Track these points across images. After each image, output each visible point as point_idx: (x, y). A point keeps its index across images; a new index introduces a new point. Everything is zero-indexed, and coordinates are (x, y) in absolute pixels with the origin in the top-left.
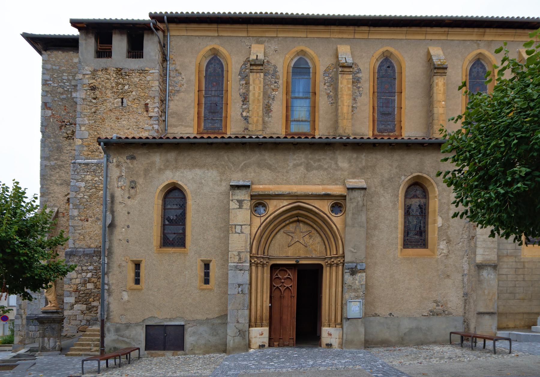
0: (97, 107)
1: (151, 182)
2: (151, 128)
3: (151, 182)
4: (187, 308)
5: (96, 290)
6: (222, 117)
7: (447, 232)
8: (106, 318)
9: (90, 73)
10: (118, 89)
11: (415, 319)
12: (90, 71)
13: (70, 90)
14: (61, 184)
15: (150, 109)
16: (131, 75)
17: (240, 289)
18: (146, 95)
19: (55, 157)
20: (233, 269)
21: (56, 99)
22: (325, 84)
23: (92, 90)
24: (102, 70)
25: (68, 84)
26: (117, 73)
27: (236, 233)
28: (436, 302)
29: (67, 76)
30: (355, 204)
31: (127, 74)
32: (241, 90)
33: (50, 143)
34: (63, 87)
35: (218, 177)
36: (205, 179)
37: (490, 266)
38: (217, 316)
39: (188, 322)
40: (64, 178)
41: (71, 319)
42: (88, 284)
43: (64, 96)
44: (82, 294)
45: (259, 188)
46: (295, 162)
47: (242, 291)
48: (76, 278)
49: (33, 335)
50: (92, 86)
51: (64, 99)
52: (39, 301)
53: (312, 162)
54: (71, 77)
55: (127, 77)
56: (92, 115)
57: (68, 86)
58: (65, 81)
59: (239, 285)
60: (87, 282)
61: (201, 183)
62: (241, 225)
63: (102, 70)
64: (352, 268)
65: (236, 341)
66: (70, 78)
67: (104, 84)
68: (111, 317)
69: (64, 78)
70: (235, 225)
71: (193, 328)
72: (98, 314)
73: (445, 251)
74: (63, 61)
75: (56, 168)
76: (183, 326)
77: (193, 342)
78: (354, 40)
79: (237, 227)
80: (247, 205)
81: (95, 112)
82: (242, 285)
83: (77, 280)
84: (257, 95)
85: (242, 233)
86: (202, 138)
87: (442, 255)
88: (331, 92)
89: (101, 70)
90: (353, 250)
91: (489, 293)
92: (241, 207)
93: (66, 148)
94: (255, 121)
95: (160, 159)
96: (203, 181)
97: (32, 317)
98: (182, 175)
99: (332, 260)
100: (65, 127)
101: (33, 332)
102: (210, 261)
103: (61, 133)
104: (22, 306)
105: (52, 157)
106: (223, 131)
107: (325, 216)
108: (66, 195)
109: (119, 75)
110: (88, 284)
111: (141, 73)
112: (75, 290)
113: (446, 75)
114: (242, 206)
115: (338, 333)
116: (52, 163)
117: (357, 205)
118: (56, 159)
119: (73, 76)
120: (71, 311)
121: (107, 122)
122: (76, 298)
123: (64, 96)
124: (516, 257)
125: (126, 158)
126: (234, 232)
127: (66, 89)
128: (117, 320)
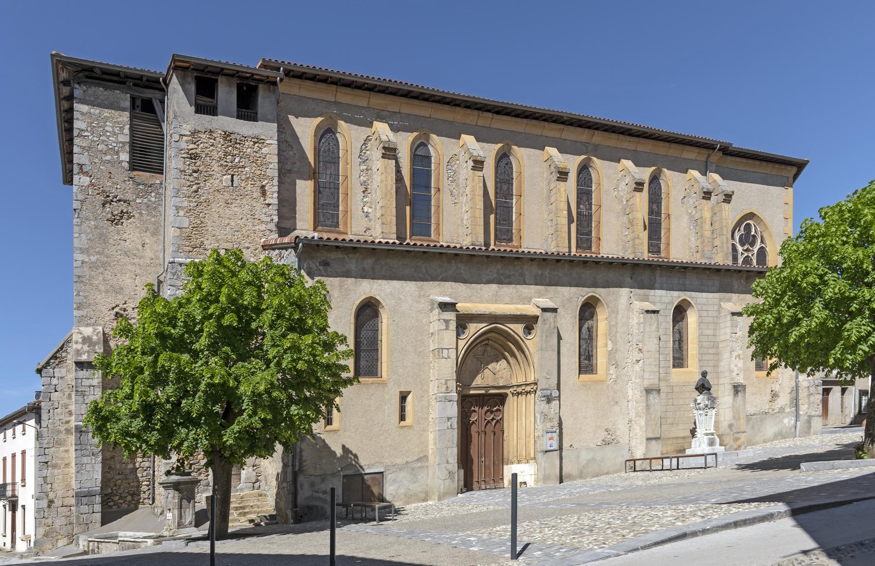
0: (199, 184)
1: (347, 295)
2: (268, 219)
3: (347, 295)
4: (386, 451)
6: (338, 211)
7: (616, 356)
8: (299, 470)
9: (190, 133)
10: (226, 162)
11: (591, 449)
12: (190, 131)
13: (116, 148)
14: (107, 292)
15: (268, 194)
16: (243, 143)
17: (449, 423)
18: (263, 173)
19: (97, 250)
20: (443, 400)
21: (96, 160)
22: (448, 179)
23: (191, 158)
24: (205, 132)
25: (113, 139)
26: (225, 139)
27: (443, 358)
28: (607, 430)
29: (112, 127)
30: (548, 326)
31: (238, 141)
32: (362, 178)
33: (89, 227)
34: (106, 143)
35: (416, 292)
36: (404, 294)
37: (655, 390)
38: (416, 458)
39: (387, 467)
40: (111, 283)
43: (108, 157)
45: (464, 307)
46: (488, 278)
47: (451, 425)
49: (86, 520)
50: (193, 154)
51: (109, 162)
52: (93, 467)
53: (503, 278)
54: (118, 128)
55: (238, 146)
56: (193, 195)
57: (114, 142)
58: (108, 134)
59: (449, 419)
61: (399, 299)
62: (448, 349)
63: (205, 132)
64: (548, 396)
65: (446, 484)
66: (117, 130)
67: (209, 152)
68: (304, 468)
69: (107, 128)
70: (442, 349)
71: (392, 475)
72: (209, 477)
73: (613, 377)
74: (106, 103)
75: (98, 266)
76: (382, 473)
77: (393, 492)
78: (476, 127)
79: (444, 351)
80: (453, 325)
81: (196, 191)
82: (451, 418)
84: (389, 187)
85: (449, 357)
86: (387, 243)
87: (612, 380)
88: (454, 188)
89: (203, 131)
90: (546, 375)
91: (655, 418)
92: (447, 328)
93: (113, 236)
94: (389, 221)
95: (356, 267)
96: (402, 296)
97: (84, 492)
98: (379, 287)
99: (523, 388)
100: (111, 204)
101: (86, 515)
102: (409, 392)
103: (104, 214)
104: (48, 479)
105: (93, 248)
106: (341, 230)
107: (519, 338)
108: (113, 309)
109: (228, 141)
111: (255, 143)
113: (566, 181)
114: (449, 326)
115: (533, 469)
116: (93, 258)
117: (550, 327)
118: (99, 253)
119: (120, 128)
121: (214, 207)
123: (108, 157)
124: (667, 381)
125: (318, 264)
126: (441, 357)
127: (111, 147)
128: (311, 471)
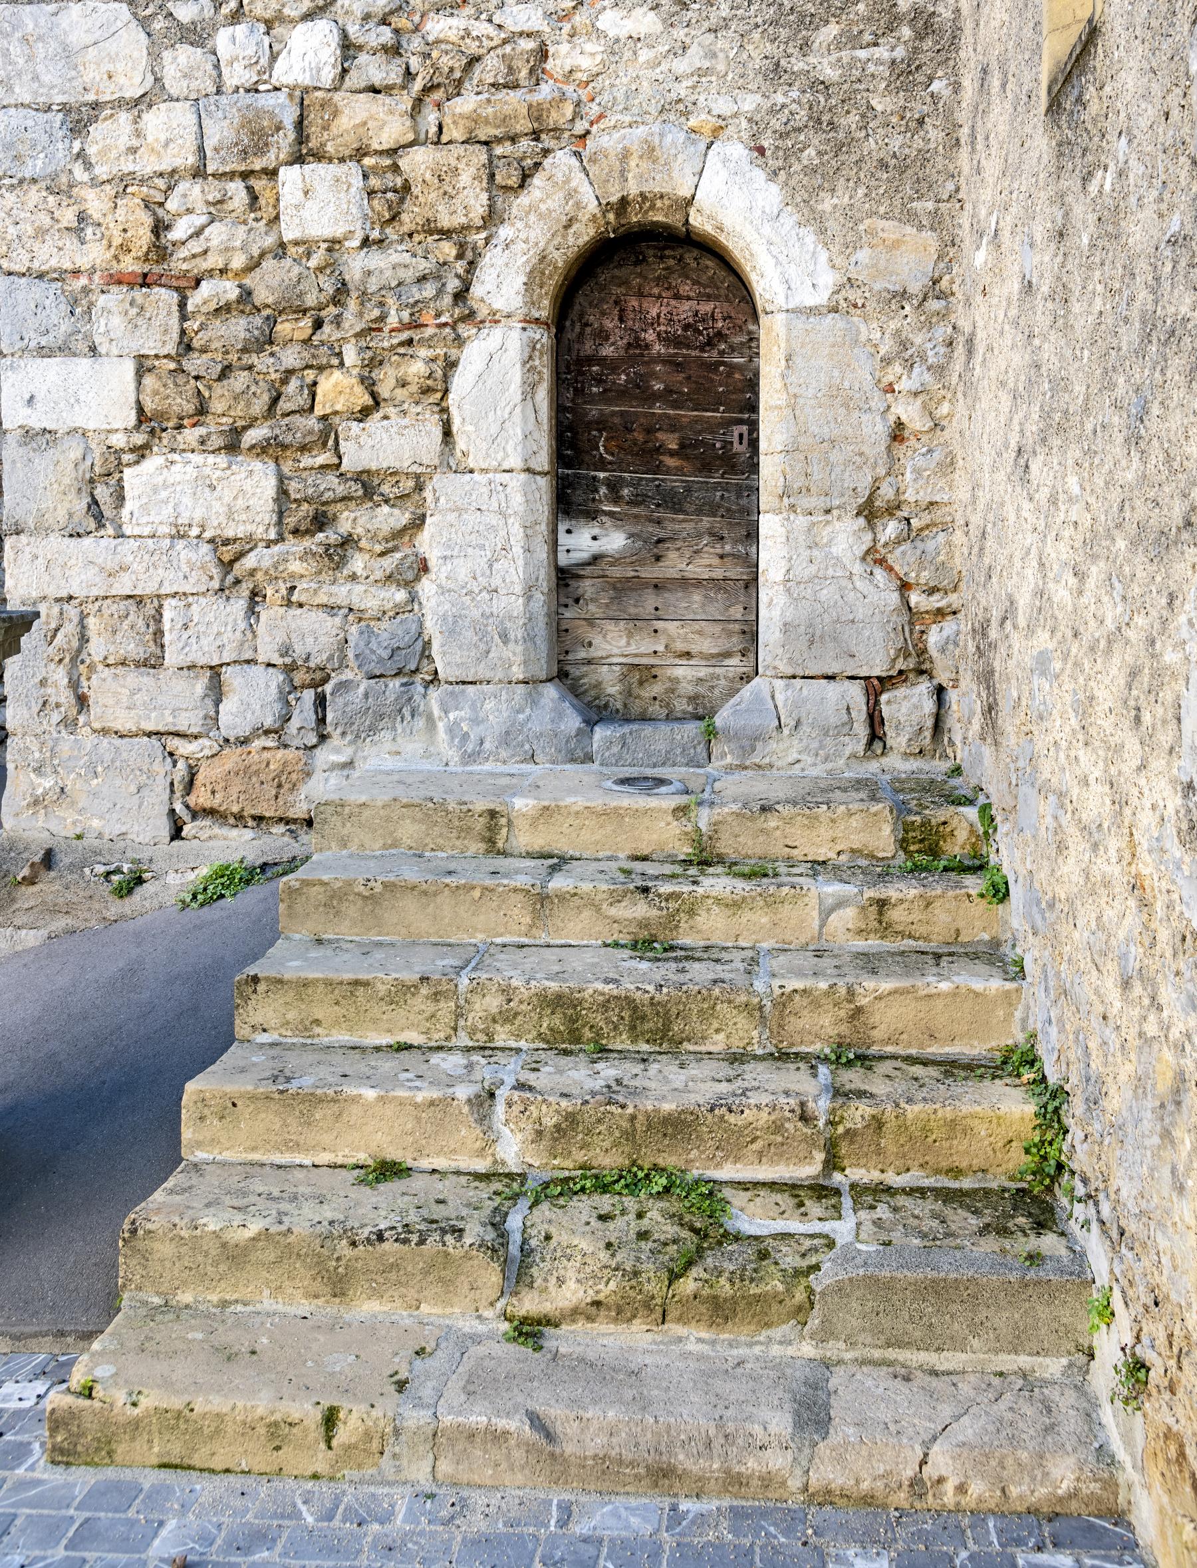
5: (396, 255)
41: (97, 648)
42: (290, 176)
44: (223, 310)
48: (139, 104)
60: (285, 141)
83: (155, 121)
110: (290, 176)
112: (129, 265)
120: (97, 547)
122: (143, 367)
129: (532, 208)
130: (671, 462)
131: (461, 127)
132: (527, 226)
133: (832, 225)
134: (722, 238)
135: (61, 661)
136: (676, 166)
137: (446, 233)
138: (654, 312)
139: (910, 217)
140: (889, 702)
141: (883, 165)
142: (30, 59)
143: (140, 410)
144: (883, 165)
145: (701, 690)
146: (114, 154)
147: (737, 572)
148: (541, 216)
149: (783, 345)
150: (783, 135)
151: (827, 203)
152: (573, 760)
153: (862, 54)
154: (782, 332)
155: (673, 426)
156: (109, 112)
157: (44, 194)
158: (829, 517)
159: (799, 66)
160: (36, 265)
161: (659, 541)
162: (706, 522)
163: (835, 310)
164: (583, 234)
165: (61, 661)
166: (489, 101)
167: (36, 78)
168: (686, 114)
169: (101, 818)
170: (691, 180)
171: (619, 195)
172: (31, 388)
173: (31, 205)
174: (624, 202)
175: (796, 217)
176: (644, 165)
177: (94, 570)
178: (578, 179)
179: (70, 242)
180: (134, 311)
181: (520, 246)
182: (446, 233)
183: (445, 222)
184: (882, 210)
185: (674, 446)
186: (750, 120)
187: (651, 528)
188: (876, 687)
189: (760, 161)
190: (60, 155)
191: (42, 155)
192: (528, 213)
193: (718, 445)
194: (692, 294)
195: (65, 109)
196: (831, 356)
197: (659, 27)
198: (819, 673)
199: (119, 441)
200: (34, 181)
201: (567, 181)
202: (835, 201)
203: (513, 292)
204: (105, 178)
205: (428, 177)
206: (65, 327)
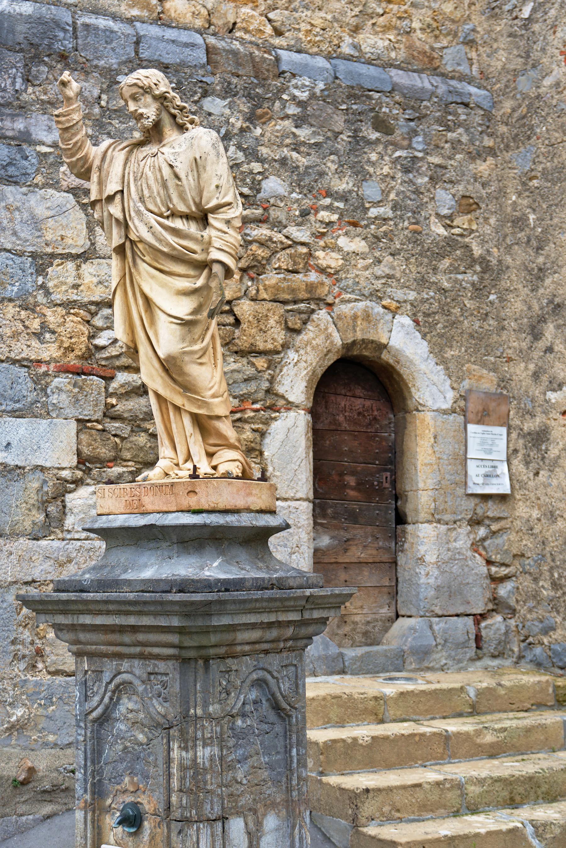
112: (72, 360)
129: (308, 343)
130: (352, 493)
131: (270, 293)
132: (306, 353)
133: (452, 366)
134: (398, 367)
135: (26, 625)
136: (380, 326)
137: (261, 353)
138: (343, 404)
139: (484, 365)
140: (486, 627)
141: (471, 336)
142: (11, 220)
143: (79, 453)
144: (471, 336)
145: (369, 628)
146: (64, 288)
147: (386, 557)
148: (313, 348)
149: (432, 430)
150: (428, 315)
151: (449, 353)
152: (333, 673)
153: (460, 277)
154: (432, 423)
155: (353, 473)
156: (60, 261)
157: (18, 309)
158: (455, 526)
159: (433, 279)
160: (12, 355)
161: (348, 540)
162: (369, 529)
163: (454, 412)
164: (332, 358)
165: (26, 625)
166: (285, 279)
167: (15, 233)
168: (380, 298)
169: (54, 734)
170: (386, 335)
171: (352, 339)
172: (8, 438)
173: (9, 316)
174: (354, 343)
175: (435, 360)
176: (365, 324)
177: (50, 563)
178: (332, 329)
179: (34, 343)
180: (76, 390)
181: (303, 364)
182: (261, 353)
183: (261, 346)
184: (472, 360)
185: (353, 483)
186: (412, 305)
187: (342, 533)
188: (479, 618)
189: (418, 328)
190: (29, 285)
191: (17, 284)
192: (306, 345)
193: (376, 483)
194: (362, 395)
195: (34, 255)
196: (454, 437)
197: (367, 250)
198: (454, 613)
199: (65, 474)
200: (10, 300)
201: (326, 329)
202: (452, 353)
203: (300, 391)
204: (59, 302)
205: (251, 319)
206: (32, 396)
